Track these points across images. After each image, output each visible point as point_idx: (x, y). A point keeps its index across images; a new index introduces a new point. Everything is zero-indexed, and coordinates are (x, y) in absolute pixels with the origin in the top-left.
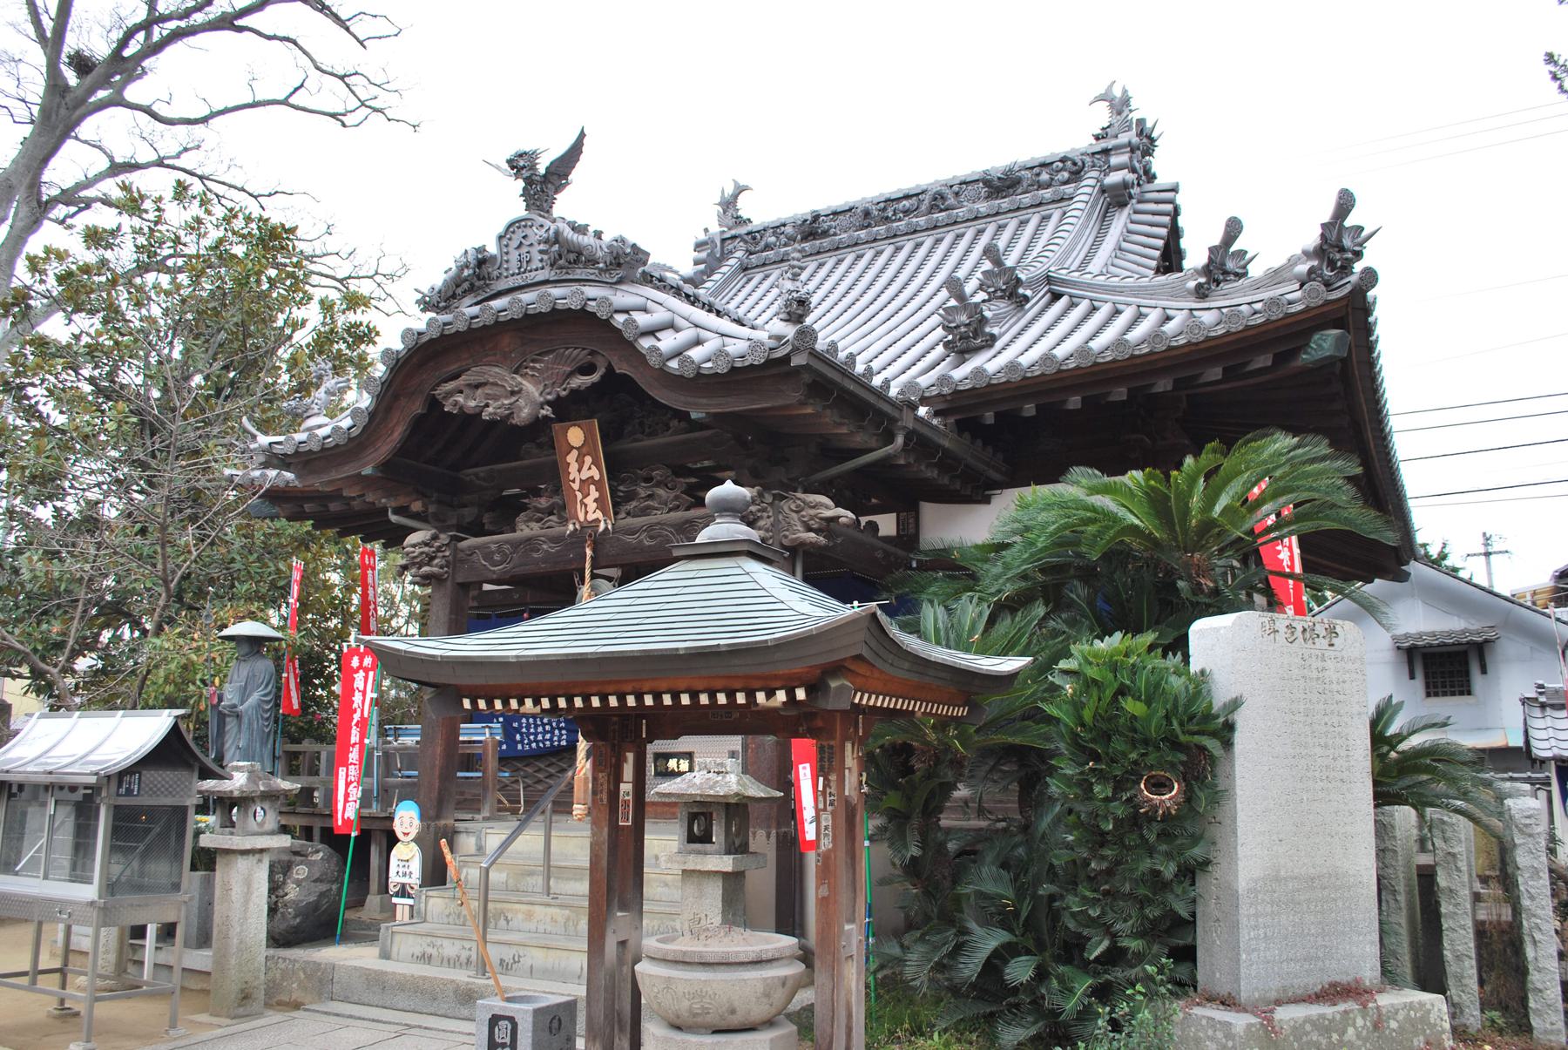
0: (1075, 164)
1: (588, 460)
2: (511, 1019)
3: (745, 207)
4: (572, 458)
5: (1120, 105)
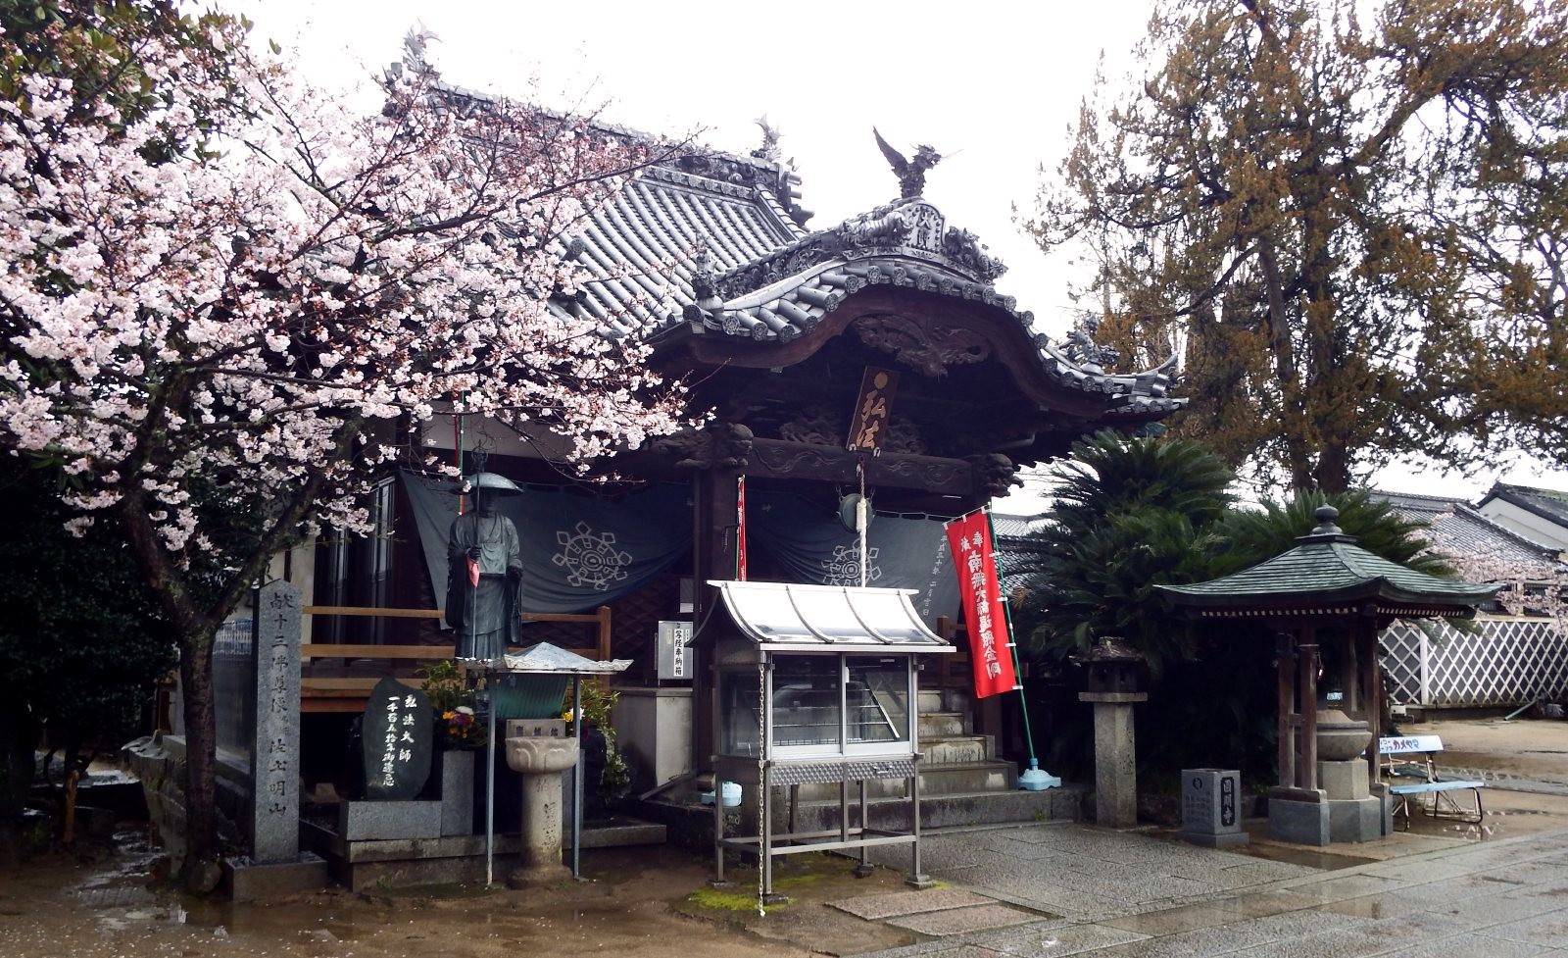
0: (748, 171)
1: (882, 400)
2: (1231, 779)
3: (431, 55)
4: (871, 396)
5: (771, 138)
